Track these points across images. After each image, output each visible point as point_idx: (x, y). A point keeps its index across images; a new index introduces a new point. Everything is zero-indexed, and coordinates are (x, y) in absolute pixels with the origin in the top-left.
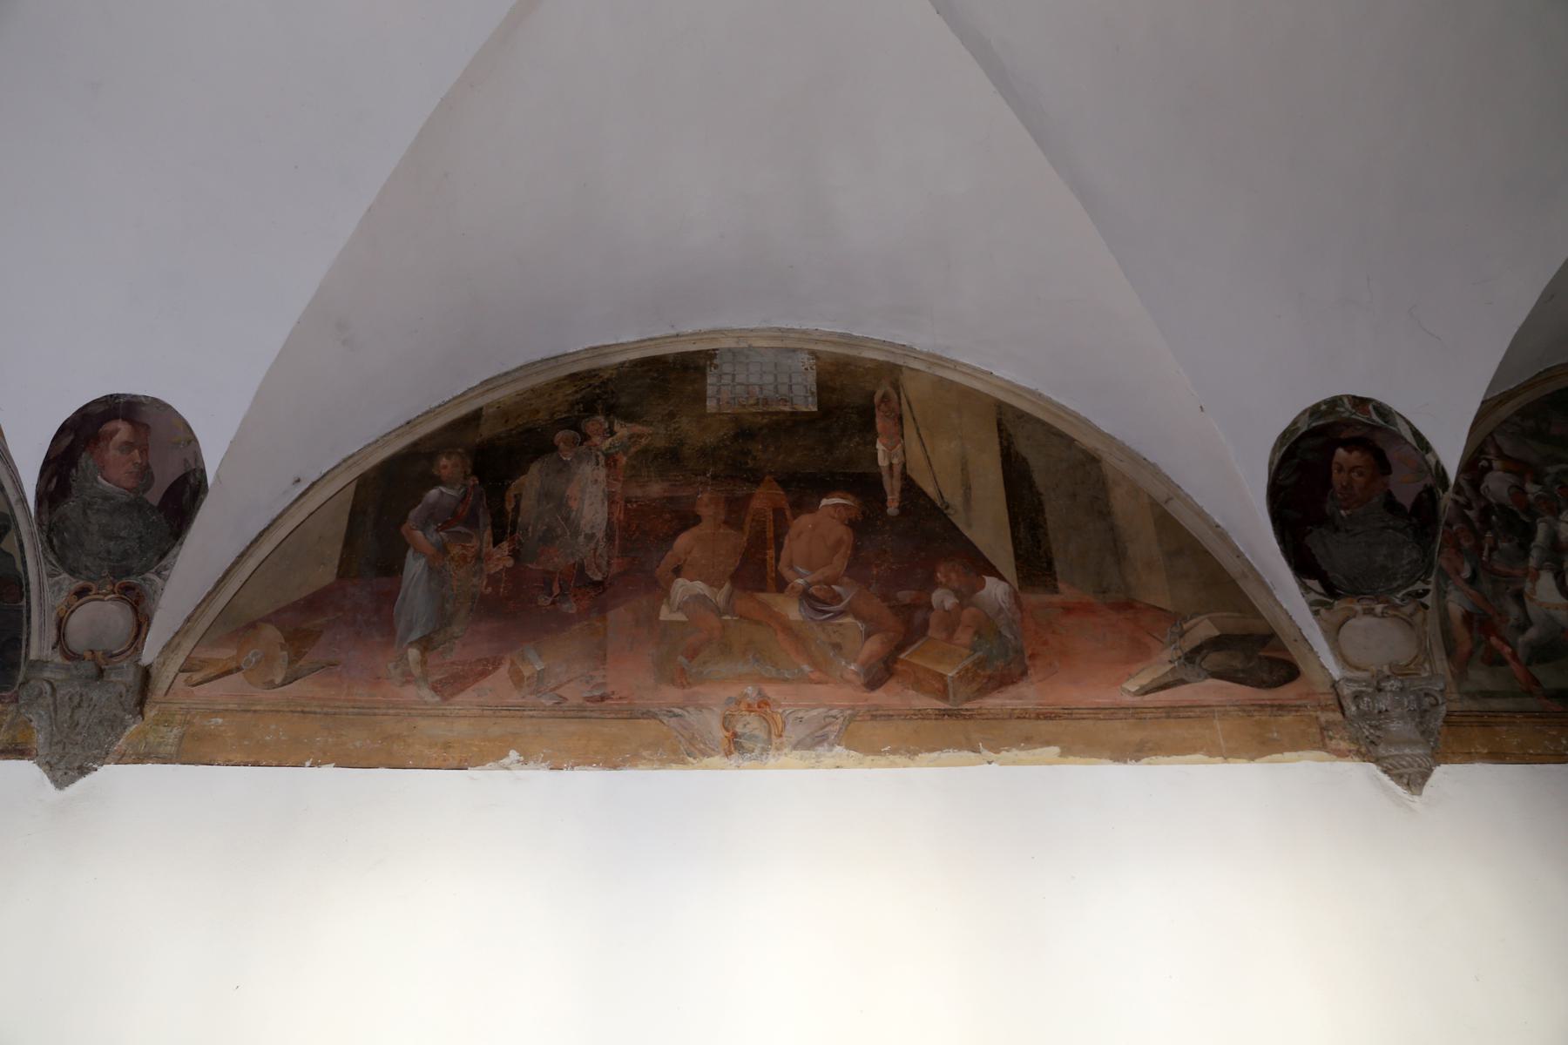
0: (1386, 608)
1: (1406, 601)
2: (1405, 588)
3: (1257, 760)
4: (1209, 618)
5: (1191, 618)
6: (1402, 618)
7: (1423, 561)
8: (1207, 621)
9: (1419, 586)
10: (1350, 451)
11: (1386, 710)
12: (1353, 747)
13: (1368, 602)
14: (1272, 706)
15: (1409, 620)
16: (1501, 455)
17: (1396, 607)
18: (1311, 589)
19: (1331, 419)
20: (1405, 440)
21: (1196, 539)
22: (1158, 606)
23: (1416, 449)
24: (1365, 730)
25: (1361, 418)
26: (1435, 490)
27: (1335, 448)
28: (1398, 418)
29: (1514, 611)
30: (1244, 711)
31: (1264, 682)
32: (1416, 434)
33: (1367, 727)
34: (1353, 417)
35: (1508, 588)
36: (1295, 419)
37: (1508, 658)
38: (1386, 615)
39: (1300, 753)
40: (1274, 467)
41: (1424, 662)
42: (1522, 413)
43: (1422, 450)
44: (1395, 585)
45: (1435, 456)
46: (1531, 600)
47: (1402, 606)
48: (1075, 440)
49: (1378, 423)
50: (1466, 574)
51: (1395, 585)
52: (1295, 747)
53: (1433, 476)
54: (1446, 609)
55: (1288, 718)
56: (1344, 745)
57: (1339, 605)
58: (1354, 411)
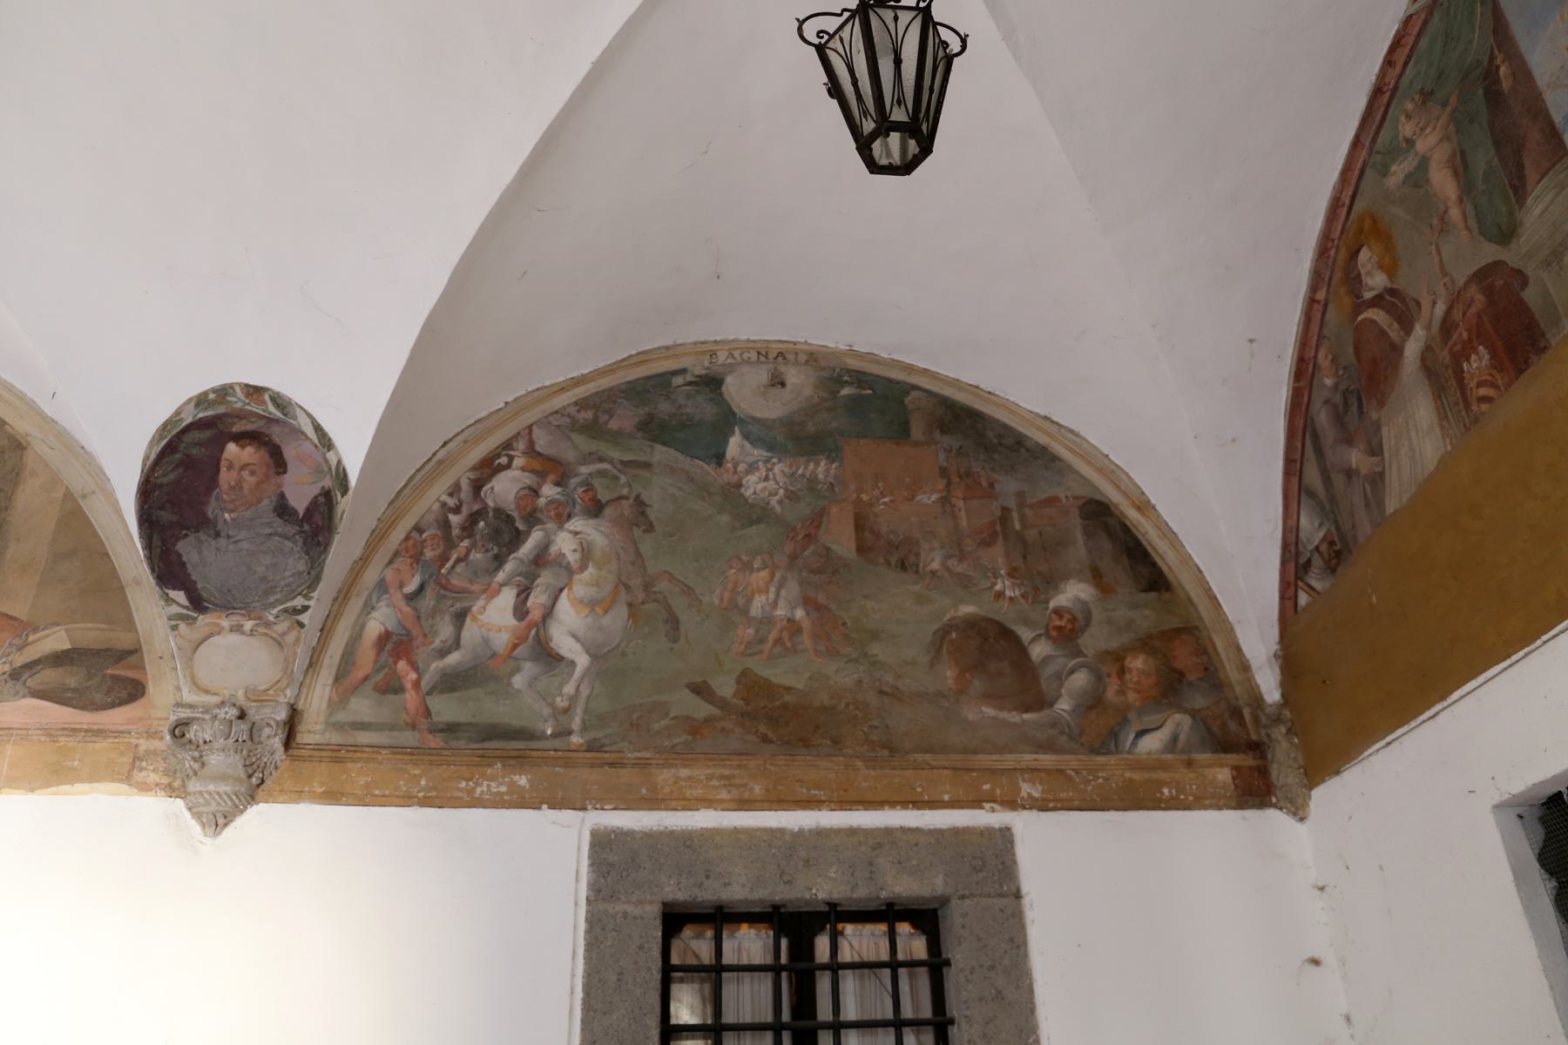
0: (256, 625)
1: (282, 618)
2: (281, 604)
3: (38, 792)
4: (67, 631)
5: (43, 630)
6: (272, 638)
7: (309, 573)
8: (63, 633)
9: (299, 602)
10: (242, 447)
11: (210, 741)
12: (165, 780)
13: (239, 618)
14: (86, 731)
15: (279, 639)
16: (531, 451)
17: (268, 625)
18: (174, 601)
19: (221, 410)
20: (306, 435)
21: (101, 540)
22: (10, 614)
23: (316, 446)
24: (186, 762)
25: (258, 410)
26: (333, 493)
27: (226, 443)
28: (298, 410)
29: (446, 631)
30: (49, 735)
31: (93, 703)
32: (318, 428)
33: (189, 758)
34: (248, 407)
35: (452, 606)
36: (178, 409)
37: (408, 686)
38: (254, 633)
39: (95, 785)
40: (149, 463)
41: (286, 688)
42: (582, 404)
43: (324, 448)
44: (272, 599)
45: (337, 454)
46: (475, 619)
47: (275, 624)
48: (6, 423)
49: (275, 415)
50: (411, 587)
51: (272, 599)
52: (91, 778)
53: (332, 477)
54: (363, 627)
55: (101, 745)
56: (153, 777)
57: (204, 620)
58: (247, 401)
